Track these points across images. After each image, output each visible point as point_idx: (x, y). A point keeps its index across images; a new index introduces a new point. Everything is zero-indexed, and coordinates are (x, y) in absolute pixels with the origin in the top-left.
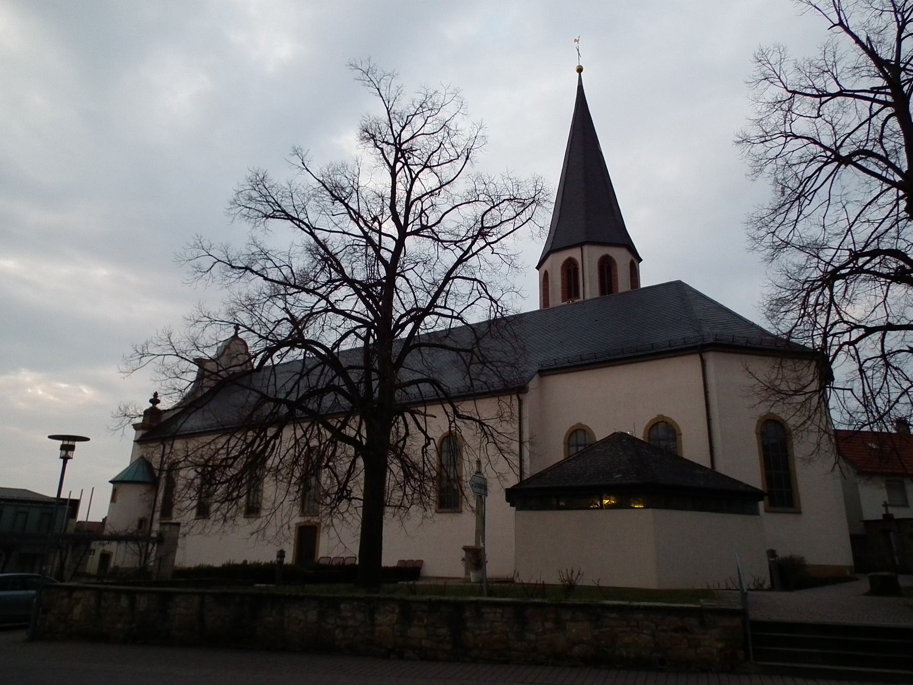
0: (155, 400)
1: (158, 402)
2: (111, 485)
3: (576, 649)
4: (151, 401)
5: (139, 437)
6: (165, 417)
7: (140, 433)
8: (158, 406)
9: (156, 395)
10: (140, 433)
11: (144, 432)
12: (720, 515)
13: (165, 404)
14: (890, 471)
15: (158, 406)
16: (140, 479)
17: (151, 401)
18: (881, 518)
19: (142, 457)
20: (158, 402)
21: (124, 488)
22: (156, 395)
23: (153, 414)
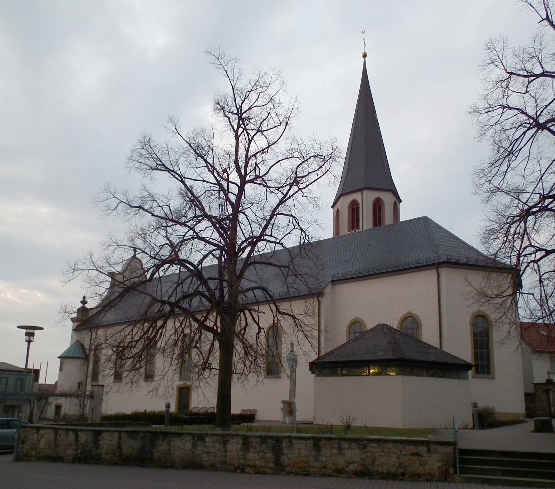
0: (84, 302)
1: (86, 303)
2: (59, 359)
6: (91, 313)
8: (86, 305)
9: (84, 298)
10: (76, 324)
11: (78, 323)
13: (91, 304)
15: (86, 305)
16: (78, 356)
17: (81, 302)
20: (86, 303)
21: (67, 361)
22: (84, 298)
23: (83, 311)
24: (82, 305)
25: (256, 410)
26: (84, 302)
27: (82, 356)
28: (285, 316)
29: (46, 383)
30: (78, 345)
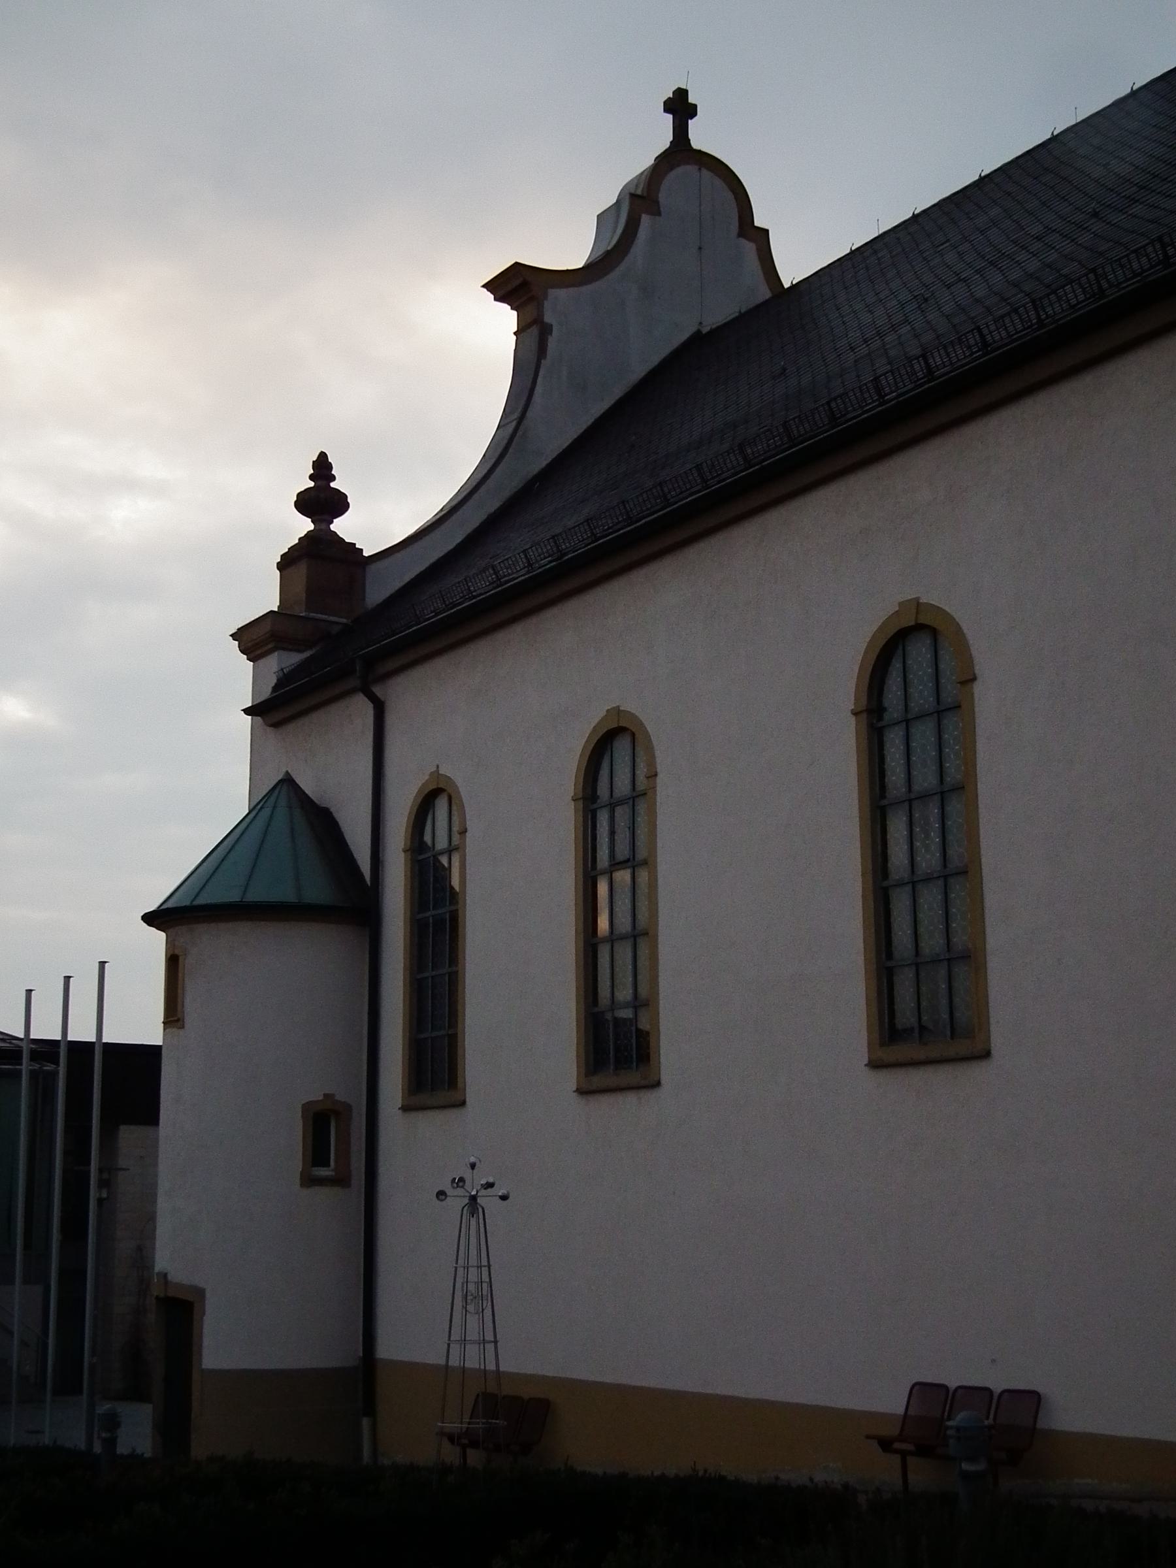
0: (322, 499)
1: (339, 504)
2: (157, 939)
3: (960, 1417)
4: (305, 503)
5: (266, 693)
6: (377, 592)
7: (274, 663)
8: (341, 526)
9: (322, 468)
10: (274, 663)
11: (293, 659)
12: (467, 1067)
13: (378, 521)
14: (603, 923)
15: (341, 526)
16: (285, 893)
17: (305, 503)
18: (321, 1098)
19: (288, 782)
20: (339, 504)
21: (214, 945)
22: (322, 468)
23: (320, 561)
24: (305, 525)
25: (875, 1065)
26: (322, 499)
27: (318, 890)
28: (514, 423)
29: (106, 1039)
30: (288, 812)
